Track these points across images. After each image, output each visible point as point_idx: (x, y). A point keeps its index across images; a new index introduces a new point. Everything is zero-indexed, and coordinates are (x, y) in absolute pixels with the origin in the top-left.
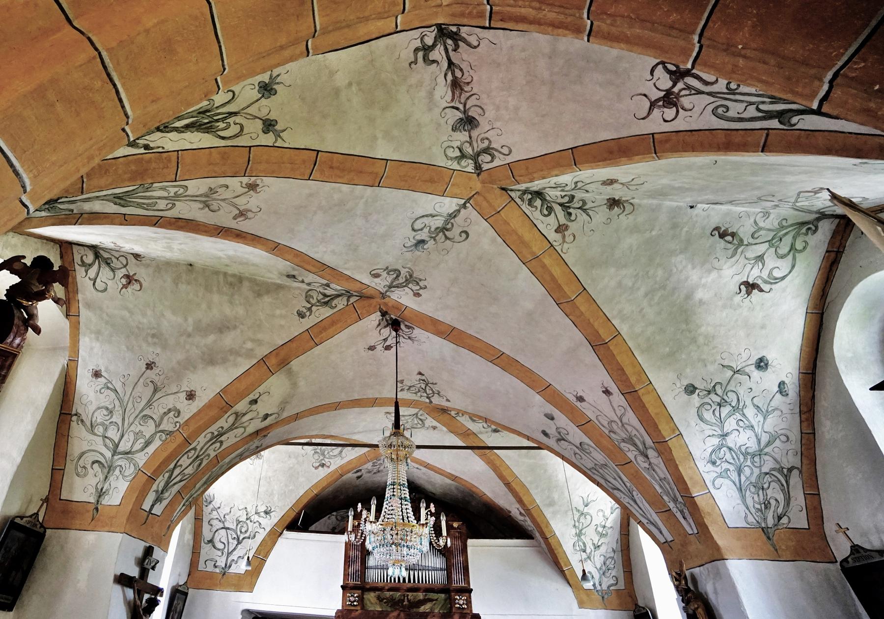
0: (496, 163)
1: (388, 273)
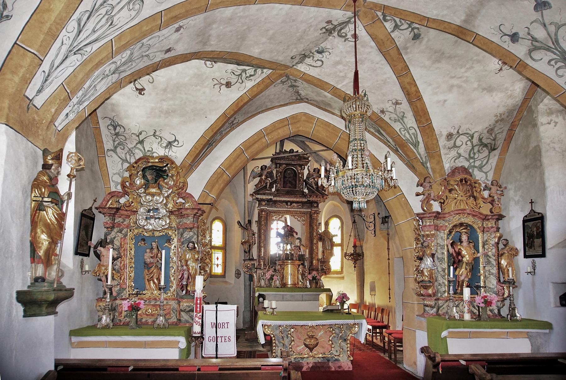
0: (280, 80)
1: (346, 35)
